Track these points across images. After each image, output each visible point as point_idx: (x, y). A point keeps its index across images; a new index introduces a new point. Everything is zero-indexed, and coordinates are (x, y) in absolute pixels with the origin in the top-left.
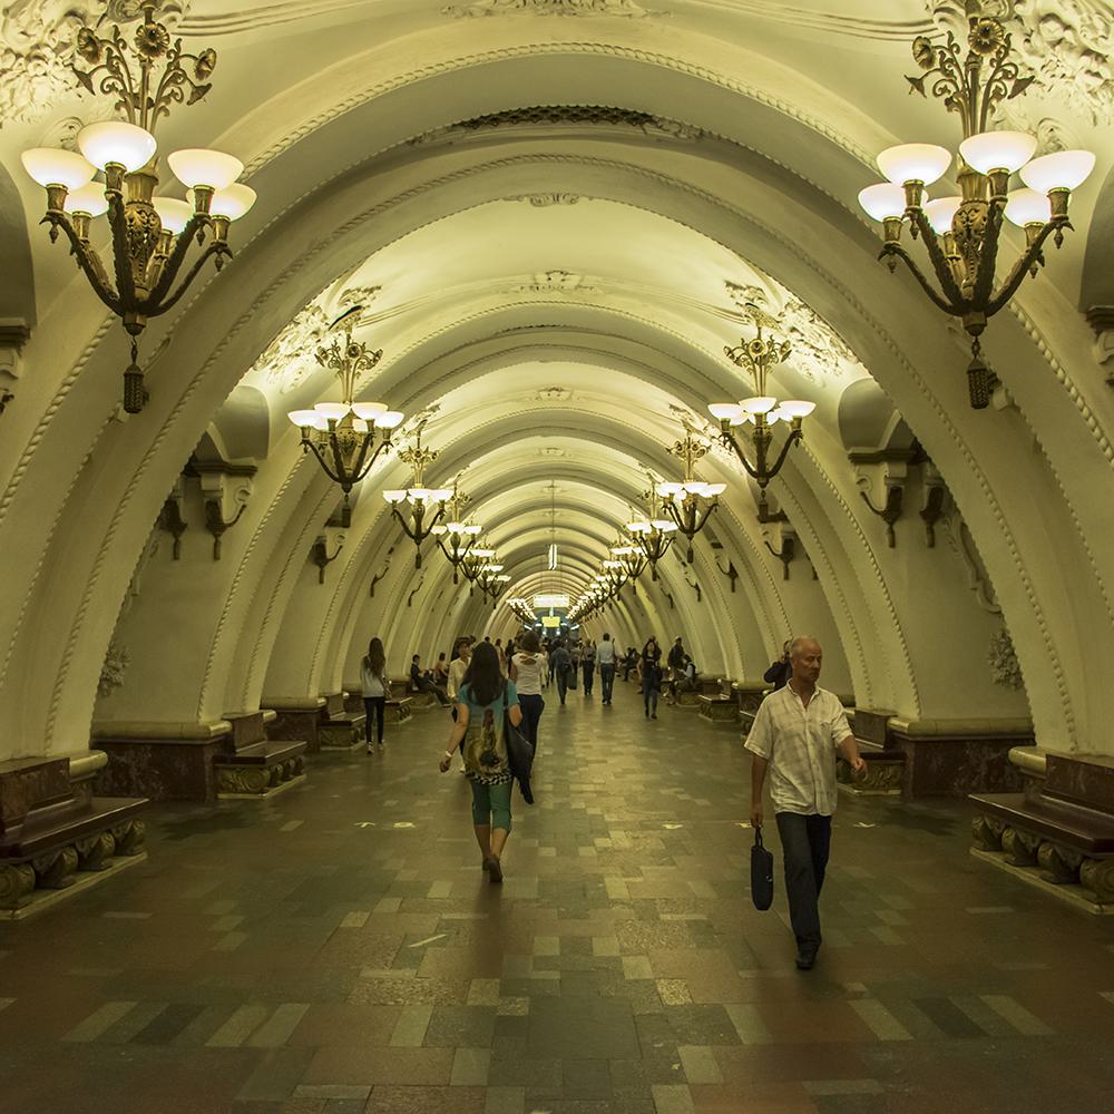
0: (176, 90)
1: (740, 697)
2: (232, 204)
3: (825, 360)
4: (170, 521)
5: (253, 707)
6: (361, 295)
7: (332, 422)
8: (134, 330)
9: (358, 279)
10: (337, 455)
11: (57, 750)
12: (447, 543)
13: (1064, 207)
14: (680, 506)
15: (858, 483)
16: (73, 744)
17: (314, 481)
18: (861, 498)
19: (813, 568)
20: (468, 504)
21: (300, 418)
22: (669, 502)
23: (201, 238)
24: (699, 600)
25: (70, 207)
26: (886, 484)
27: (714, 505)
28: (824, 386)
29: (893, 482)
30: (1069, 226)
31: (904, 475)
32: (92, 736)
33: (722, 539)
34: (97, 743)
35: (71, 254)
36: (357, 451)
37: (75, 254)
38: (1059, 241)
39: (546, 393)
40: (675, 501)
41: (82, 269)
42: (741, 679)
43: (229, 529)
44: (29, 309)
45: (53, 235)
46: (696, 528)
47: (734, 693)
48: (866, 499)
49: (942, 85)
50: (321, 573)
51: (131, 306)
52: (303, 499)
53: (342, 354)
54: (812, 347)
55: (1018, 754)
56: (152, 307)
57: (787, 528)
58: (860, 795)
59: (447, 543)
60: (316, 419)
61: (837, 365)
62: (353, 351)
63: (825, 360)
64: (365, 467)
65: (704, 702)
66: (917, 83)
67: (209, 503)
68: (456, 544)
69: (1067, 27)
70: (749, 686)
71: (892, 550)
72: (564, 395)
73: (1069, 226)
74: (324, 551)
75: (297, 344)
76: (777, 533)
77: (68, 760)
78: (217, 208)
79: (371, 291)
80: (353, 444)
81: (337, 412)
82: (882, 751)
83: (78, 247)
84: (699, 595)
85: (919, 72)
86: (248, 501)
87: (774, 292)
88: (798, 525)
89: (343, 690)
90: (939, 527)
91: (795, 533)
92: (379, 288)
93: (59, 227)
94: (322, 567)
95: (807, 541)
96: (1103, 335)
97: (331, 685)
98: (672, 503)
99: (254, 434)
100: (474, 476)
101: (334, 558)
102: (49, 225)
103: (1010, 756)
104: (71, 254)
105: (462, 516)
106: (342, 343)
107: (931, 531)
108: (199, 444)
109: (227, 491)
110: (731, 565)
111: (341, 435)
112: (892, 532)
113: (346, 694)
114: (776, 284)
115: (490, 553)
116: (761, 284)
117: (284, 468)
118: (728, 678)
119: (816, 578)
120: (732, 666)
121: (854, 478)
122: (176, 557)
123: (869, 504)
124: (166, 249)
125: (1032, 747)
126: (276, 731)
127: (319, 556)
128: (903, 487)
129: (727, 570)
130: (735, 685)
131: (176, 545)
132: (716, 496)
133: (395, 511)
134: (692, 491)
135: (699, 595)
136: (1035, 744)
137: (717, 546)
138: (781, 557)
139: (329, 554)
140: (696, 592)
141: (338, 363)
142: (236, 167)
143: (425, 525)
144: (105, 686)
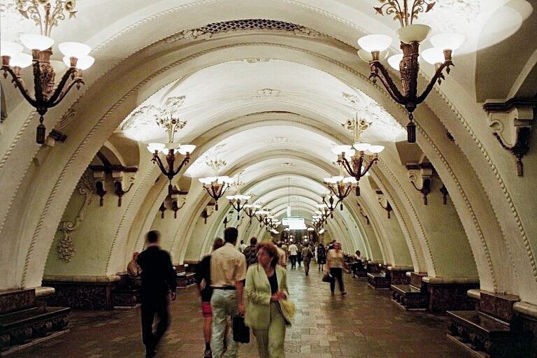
0: (61, 15)
2: (85, 64)
4: (162, 208)
5: (181, 263)
6: (177, 100)
8: (42, 112)
9: (177, 92)
10: (213, 191)
11: (28, 286)
13: (450, 58)
14: (349, 160)
16: (35, 283)
17: (206, 194)
21: (202, 181)
22: (342, 160)
23: (73, 77)
25: (12, 64)
27: (374, 160)
29: (518, 123)
30: (452, 64)
33: (383, 190)
34: (45, 283)
35: (12, 82)
36: (220, 188)
37: (14, 82)
38: (448, 70)
39: (262, 92)
40: (346, 157)
41: (18, 88)
42: (394, 265)
43: (127, 193)
45: (5, 75)
48: (498, 138)
49: (390, 9)
51: (42, 105)
59: (235, 204)
60: (208, 181)
65: (370, 277)
68: (239, 203)
71: (521, 178)
73: (452, 64)
77: (34, 290)
80: (218, 187)
81: (213, 179)
83: (161, 167)
86: (134, 181)
87: (361, 96)
93: (8, 72)
94: (102, 196)
98: (344, 159)
99: (133, 150)
102: (3, 71)
104: (12, 82)
105: (253, 202)
106: (170, 118)
107: (520, 164)
108: (93, 159)
109: (179, 199)
110: (388, 203)
114: (361, 93)
116: (355, 94)
117: (195, 195)
120: (420, 255)
123: (501, 142)
124: (57, 80)
126: (187, 270)
127: (205, 215)
129: (386, 206)
134: (360, 150)
135: (368, 221)
137: (379, 192)
138: (422, 191)
142: (88, 49)
144: (69, 6)
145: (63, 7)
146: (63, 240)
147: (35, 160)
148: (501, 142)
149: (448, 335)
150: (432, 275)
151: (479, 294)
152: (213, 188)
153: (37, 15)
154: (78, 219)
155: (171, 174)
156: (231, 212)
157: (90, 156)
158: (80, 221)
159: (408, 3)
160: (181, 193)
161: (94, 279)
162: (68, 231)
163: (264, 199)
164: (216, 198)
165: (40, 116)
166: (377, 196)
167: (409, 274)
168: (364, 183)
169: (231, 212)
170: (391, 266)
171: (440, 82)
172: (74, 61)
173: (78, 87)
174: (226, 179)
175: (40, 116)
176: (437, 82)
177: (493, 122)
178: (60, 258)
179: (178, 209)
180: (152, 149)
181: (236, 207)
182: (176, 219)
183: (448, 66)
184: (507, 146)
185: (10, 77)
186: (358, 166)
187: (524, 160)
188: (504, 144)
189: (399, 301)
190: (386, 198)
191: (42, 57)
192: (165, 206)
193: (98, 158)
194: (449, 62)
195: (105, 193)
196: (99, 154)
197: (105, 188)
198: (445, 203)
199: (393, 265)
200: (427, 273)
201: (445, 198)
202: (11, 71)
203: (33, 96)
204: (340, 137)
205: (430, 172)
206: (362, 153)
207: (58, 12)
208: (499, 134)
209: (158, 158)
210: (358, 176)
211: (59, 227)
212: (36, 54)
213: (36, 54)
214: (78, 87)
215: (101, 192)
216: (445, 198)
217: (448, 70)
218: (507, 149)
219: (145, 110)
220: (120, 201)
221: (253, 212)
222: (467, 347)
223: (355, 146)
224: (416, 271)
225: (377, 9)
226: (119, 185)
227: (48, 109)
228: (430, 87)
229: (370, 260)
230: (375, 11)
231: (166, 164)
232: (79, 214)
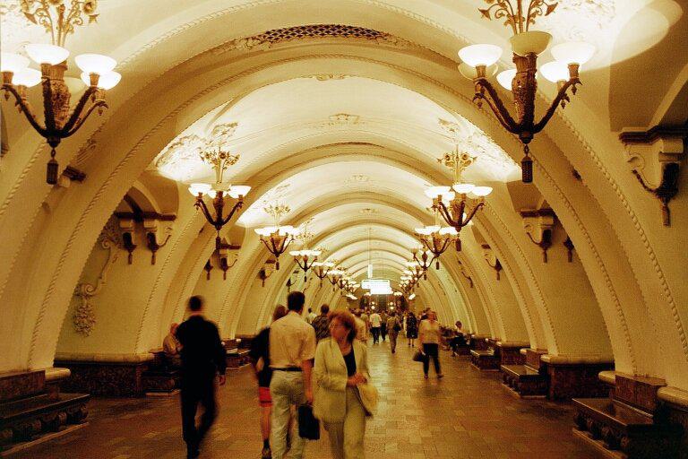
1: (502, 352)
2: (109, 82)
4: (208, 267)
6: (227, 129)
7: (240, 196)
8: (54, 144)
9: (227, 118)
10: (273, 245)
11: (36, 367)
15: (631, 161)
16: (44, 364)
17: (206, 225)
18: (635, 178)
20: (327, 254)
21: (259, 231)
23: (94, 99)
27: (479, 205)
29: (665, 158)
31: (681, 151)
32: (55, 361)
34: (58, 363)
35: (16, 105)
38: (574, 90)
39: (336, 118)
43: (163, 248)
44: (176, 209)
45: (7, 97)
47: (497, 349)
48: (639, 177)
49: (500, 12)
51: (53, 134)
53: (217, 157)
55: (605, 375)
56: (281, 252)
58: (447, 340)
60: (267, 232)
62: (223, 155)
64: (74, 127)
66: (485, 13)
70: (509, 344)
71: (666, 230)
76: (538, 226)
79: (232, 126)
81: (272, 230)
82: (651, 422)
85: (486, 6)
89: (237, 337)
90: (673, 205)
93: (10, 92)
95: (571, 227)
97: (229, 335)
99: (171, 191)
100: (326, 244)
102: (4, 91)
104: (16, 105)
106: (217, 151)
107: (667, 210)
111: (274, 238)
113: (239, 340)
115: (331, 265)
118: (534, 347)
121: (523, 224)
122: (130, 262)
123: (642, 182)
124: (73, 103)
127: (262, 275)
129: (494, 264)
130: (544, 357)
131: (130, 256)
132: (484, 67)
133: (296, 260)
134: (461, 192)
135: (472, 284)
137: (486, 247)
139: (267, 274)
141: (214, 161)
143: (309, 264)
145: (81, 9)
146: (81, 307)
147: (45, 205)
148: (642, 182)
149: (574, 430)
150: (553, 353)
151: (614, 378)
153: (47, 19)
154: (100, 280)
155: (219, 223)
157: (114, 201)
160: (232, 248)
162: (87, 296)
163: (338, 256)
164: (277, 253)
165: (51, 149)
166: (483, 252)
167: (523, 351)
168: (466, 235)
170: (500, 341)
171: (563, 106)
172: (94, 78)
173: (100, 112)
176: (560, 106)
177: (632, 156)
178: (77, 331)
180: (195, 191)
181: (303, 265)
184: (650, 187)
185: (13, 99)
186: (459, 213)
188: (646, 184)
189: (511, 387)
190: (494, 255)
191: (53, 73)
192: (211, 264)
194: (575, 80)
195: (134, 247)
196: (127, 198)
198: (570, 260)
199: (504, 339)
200: (546, 350)
201: (570, 254)
202: (13, 91)
203: (42, 123)
204: (436, 176)
205: (550, 221)
206: (464, 196)
207: (74, 16)
208: (639, 172)
209: (203, 202)
210: (459, 225)
211: (75, 291)
212: (46, 69)
213: (46, 69)
214: (100, 112)
215: (129, 246)
216: (570, 254)
217: (574, 90)
218: (650, 190)
220: (225, 274)
221: (325, 272)
222: (598, 444)
223: (455, 187)
224: (534, 347)
225: (483, 12)
226: (151, 237)
227: (62, 139)
228: (551, 111)
229: (474, 333)
230: (481, 14)
231: (212, 211)
232: (101, 274)
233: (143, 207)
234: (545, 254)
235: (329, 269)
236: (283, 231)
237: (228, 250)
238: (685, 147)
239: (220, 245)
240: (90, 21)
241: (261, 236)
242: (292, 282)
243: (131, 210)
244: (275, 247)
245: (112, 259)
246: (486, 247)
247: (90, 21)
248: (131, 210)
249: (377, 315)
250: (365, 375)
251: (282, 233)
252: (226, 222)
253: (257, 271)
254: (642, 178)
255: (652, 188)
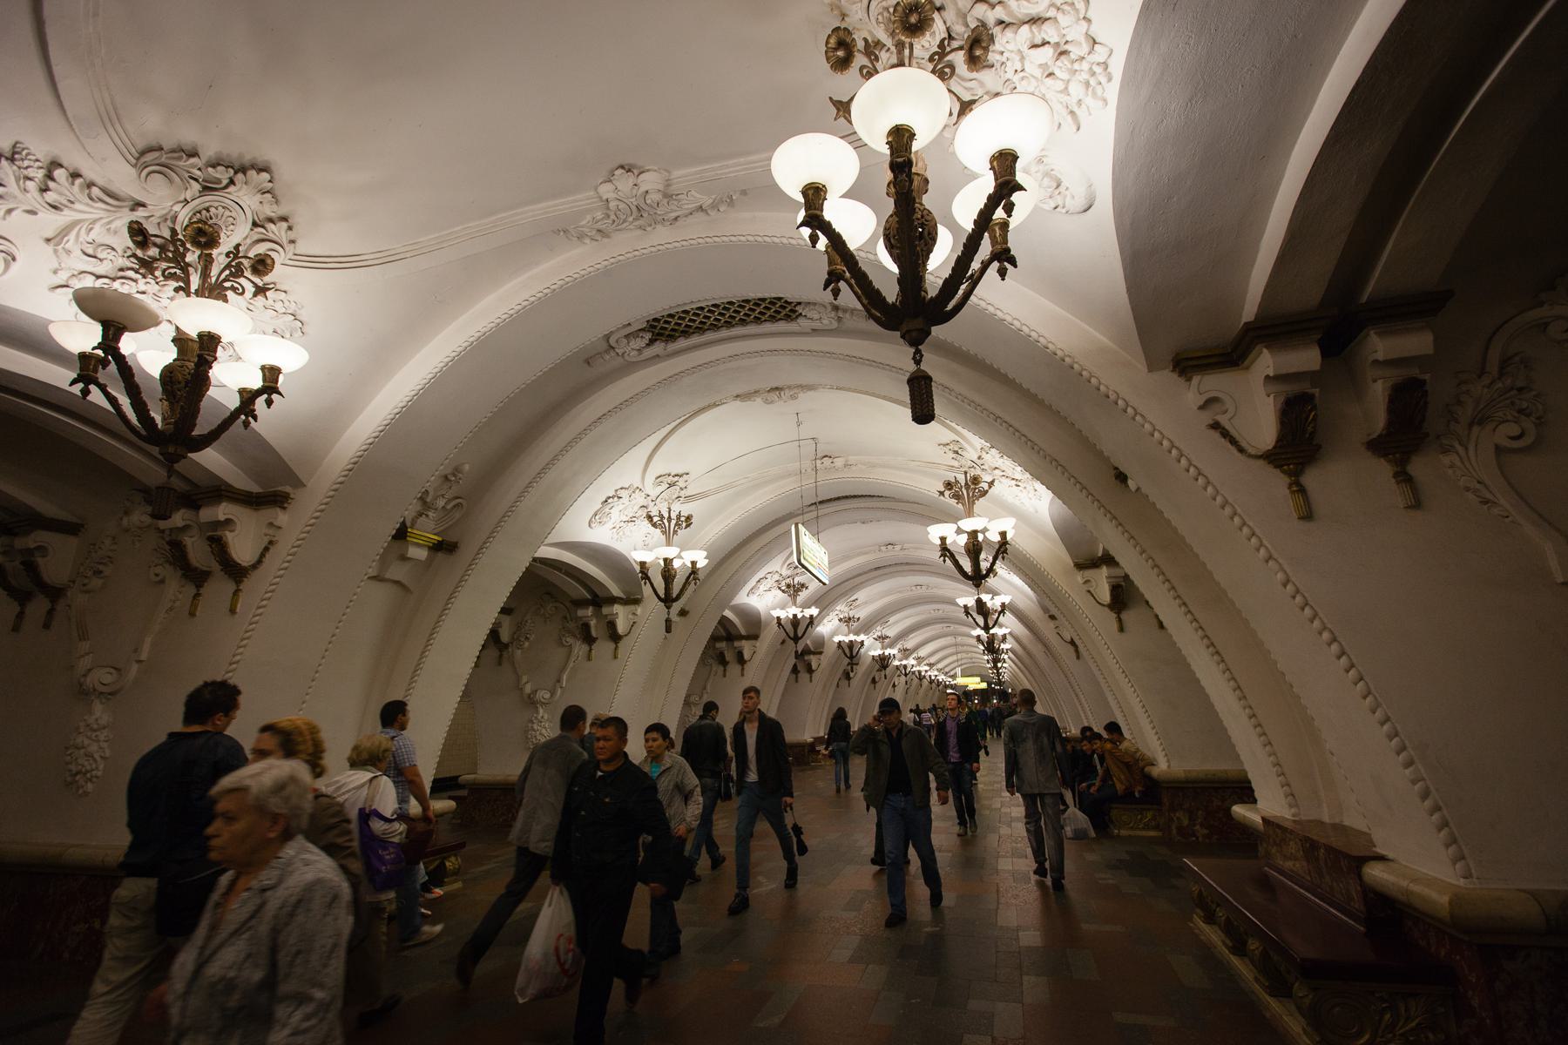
2: (702, 563)
3: (1025, 488)
4: (795, 670)
12: (902, 668)
13: (1005, 538)
15: (1201, 408)
18: (1216, 435)
19: (1157, 616)
24: (1078, 657)
26: (1108, 582)
28: (1037, 512)
33: (1056, 613)
46: (800, 635)
48: (1225, 434)
50: (811, 677)
52: (871, 667)
54: (1013, 479)
55: (1238, 810)
57: (1116, 572)
59: (902, 668)
61: (1036, 490)
63: (1025, 488)
67: (582, 625)
69: (1003, 471)
72: (898, 548)
73: (280, 394)
74: (811, 666)
75: (769, 586)
76: (1101, 581)
78: (698, 566)
83: (844, 651)
84: (1077, 651)
88: (1131, 563)
91: (1126, 577)
92: (688, 474)
94: (616, 643)
96: (1196, 380)
99: (754, 625)
101: (260, 562)
103: (1232, 813)
107: (1299, 490)
112: (1120, 621)
117: (769, 636)
119: (1161, 626)
121: (1080, 579)
125: (1252, 806)
127: (874, 681)
128: (1316, 391)
131: (725, 670)
133: (897, 668)
135: (1077, 651)
136: (1255, 801)
137: (1052, 617)
138: (1272, 457)
140: (1072, 649)
152: (881, 659)
154: (704, 691)
155: (796, 639)
156: (899, 676)
158: (561, 687)
159: (873, 4)
160: (748, 638)
161: (795, 741)
166: (1052, 624)
169: (899, 676)
174: (862, 637)
175: (913, 350)
179: (813, 671)
180: (837, 639)
181: (662, 593)
182: (725, 679)
183: (270, 395)
187: (1124, 616)
193: (720, 628)
195: (799, 672)
196: (720, 622)
197: (596, 630)
217: (269, 403)
218: (1103, 605)
219: (622, 493)
221: (923, 674)
226: (612, 625)
227: (674, 604)
231: (847, 651)
233: (733, 632)
234: (1302, 490)
235: (926, 671)
236: (887, 652)
237: (744, 641)
238: (1322, 365)
239: (800, 656)
240: (255, 295)
241: (778, 618)
242: (877, 679)
243: (724, 634)
244: (883, 662)
245: (713, 673)
246: (1052, 617)
247: (255, 295)
248: (724, 634)
249: (870, 966)
250: (996, 714)
251: (886, 654)
252: (802, 637)
253: (870, 680)
254: (1233, 432)
255: (1105, 603)
